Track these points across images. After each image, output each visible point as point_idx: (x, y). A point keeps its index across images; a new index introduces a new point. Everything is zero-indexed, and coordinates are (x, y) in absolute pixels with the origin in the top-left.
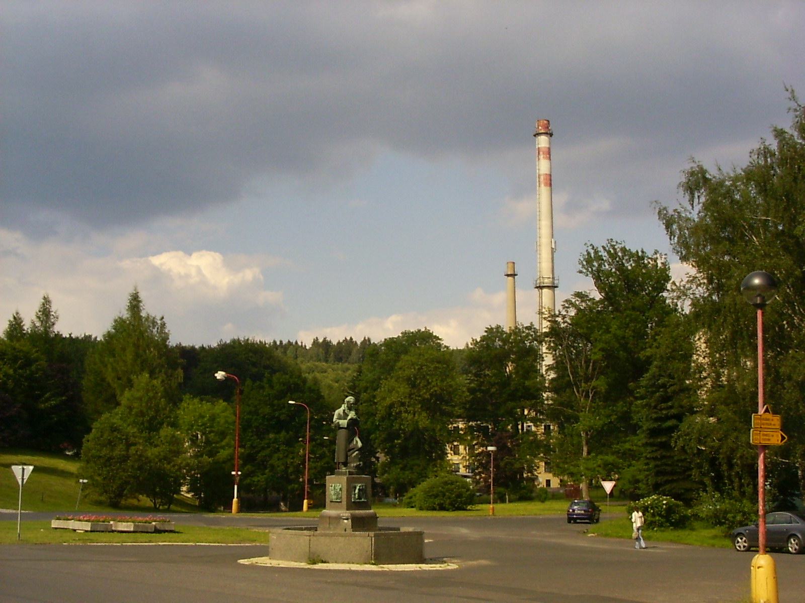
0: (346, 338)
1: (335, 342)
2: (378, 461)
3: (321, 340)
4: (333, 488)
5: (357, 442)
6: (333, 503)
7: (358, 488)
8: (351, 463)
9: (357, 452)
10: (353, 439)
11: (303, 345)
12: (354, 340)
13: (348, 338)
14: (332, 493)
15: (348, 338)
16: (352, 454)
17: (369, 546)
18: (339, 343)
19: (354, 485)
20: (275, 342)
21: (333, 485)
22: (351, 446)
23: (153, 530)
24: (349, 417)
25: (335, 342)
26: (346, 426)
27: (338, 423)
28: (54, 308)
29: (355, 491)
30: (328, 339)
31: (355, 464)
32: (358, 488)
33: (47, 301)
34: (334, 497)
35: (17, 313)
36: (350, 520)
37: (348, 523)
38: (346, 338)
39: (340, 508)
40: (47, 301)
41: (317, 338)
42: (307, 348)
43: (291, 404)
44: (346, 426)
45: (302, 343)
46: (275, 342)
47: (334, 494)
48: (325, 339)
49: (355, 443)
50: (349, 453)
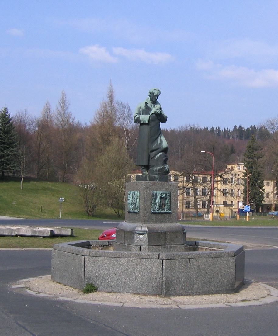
0: (251, 126)
1: (246, 128)
2: (264, 191)
3: (238, 127)
4: (131, 196)
5: (161, 142)
6: (131, 214)
7: (159, 196)
8: (153, 166)
9: (161, 153)
10: (157, 138)
11: (229, 130)
12: (256, 127)
13: (253, 126)
14: (130, 201)
15: (253, 126)
16: (155, 156)
17: (158, 271)
18: (248, 129)
19: (154, 192)
20: (213, 128)
21: (132, 193)
22: (154, 146)
23: (49, 234)
24: (152, 112)
25: (246, 128)
26: (147, 122)
27: (139, 117)
28: (68, 98)
29: (155, 200)
30: (242, 126)
31: (158, 168)
32: (159, 196)
33: (64, 94)
34: (132, 207)
35: (48, 103)
36: (146, 236)
37: (143, 239)
38: (251, 126)
39: (138, 221)
40: (64, 94)
41: (236, 126)
42: (231, 131)
43: (202, 152)
44: (147, 122)
45: (228, 128)
46: (213, 128)
47: (132, 204)
48: (240, 126)
49: (159, 142)
50: (152, 154)
